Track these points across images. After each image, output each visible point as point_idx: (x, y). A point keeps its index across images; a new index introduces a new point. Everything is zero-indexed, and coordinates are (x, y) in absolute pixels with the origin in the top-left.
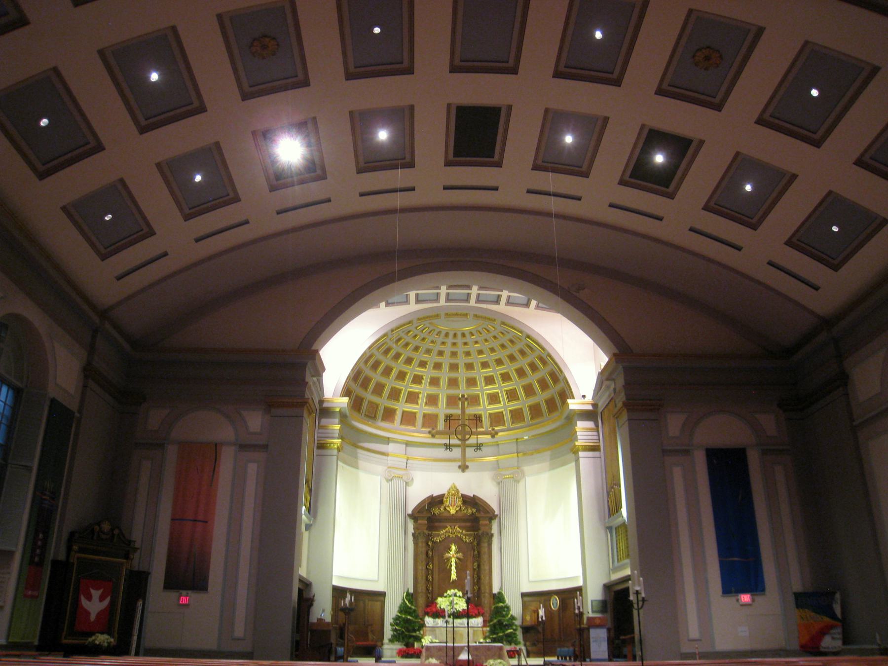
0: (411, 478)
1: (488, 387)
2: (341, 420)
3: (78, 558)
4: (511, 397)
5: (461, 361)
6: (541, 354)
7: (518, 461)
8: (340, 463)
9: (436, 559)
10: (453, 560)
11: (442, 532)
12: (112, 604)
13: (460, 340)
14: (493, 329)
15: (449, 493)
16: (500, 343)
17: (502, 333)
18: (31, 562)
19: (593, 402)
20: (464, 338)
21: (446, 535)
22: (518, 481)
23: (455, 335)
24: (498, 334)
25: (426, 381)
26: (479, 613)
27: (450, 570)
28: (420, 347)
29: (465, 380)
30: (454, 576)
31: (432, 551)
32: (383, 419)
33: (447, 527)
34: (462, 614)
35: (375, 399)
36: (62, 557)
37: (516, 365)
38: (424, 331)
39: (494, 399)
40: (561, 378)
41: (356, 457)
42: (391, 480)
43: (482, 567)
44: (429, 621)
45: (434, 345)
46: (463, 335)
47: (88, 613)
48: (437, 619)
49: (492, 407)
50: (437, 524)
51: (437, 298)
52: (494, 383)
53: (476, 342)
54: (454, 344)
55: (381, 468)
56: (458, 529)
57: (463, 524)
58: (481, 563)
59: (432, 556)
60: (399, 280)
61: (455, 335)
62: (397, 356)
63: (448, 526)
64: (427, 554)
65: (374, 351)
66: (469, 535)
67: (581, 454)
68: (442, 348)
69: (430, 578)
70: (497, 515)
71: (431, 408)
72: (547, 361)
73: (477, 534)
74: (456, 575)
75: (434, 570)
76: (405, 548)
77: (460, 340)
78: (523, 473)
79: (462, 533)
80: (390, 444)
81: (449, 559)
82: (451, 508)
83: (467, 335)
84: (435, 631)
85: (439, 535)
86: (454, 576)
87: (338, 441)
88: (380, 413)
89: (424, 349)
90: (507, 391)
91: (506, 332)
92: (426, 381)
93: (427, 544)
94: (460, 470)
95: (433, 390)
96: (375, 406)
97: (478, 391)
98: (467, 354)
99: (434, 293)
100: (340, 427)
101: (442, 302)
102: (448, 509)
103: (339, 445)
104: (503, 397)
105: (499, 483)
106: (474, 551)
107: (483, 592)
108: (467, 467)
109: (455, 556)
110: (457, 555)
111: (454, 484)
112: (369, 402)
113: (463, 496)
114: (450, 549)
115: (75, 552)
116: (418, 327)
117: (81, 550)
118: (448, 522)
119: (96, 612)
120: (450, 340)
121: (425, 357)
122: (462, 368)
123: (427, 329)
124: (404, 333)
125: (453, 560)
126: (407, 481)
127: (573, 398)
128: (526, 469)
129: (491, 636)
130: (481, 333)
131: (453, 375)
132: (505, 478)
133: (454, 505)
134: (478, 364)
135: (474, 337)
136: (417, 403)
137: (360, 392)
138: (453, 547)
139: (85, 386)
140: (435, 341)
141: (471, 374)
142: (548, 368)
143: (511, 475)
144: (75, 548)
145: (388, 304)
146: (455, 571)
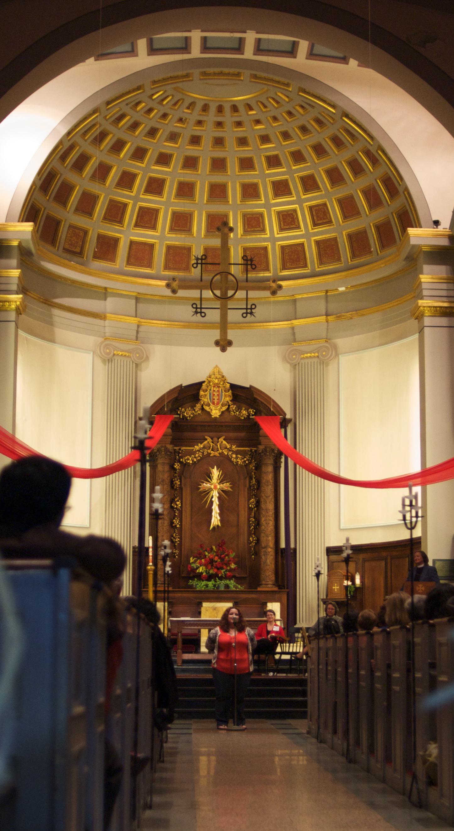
2: (21, 259)
4: (318, 217)
6: (368, 146)
8: (20, 332)
9: (187, 493)
11: (197, 448)
13: (228, 118)
14: (287, 99)
16: (300, 123)
17: (302, 107)
19: (451, 233)
20: (236, 114)
21: (203, 453)
23: (220, 109)
25: (170, 189)
31: (181, 479)
32: (96, 256)
33: (206, 439)
35: (81, 221)
38: (165, 103)
40: (401, 189)
41: (51, 323)
43: (263, 506)
45: (184, 126)
46: (235, 108)
50: (188, 434)
51: (185, 47)
52: (289, 193)
53: (258, 122)
55: (91, 340)
56: (224, 442)
57: (232, 435)
58: (262, 500)
59: (181, 488)
60: (105, 25)
61: (220, 109)
62: (118, 146)
63: (206, 437)
64: (172, 482)
65: (56, 164)
66: (243, 454)
67: (427, 321)
68: (197, 131)
69: (176, 522)
70: (290, 420)
71: (179, 236)
72: (379, 158)
73: (256, 451)
74: (219, 518)
75: (183, 510)
77: (228, 118)
79: (230, 450)
80: (109, 299)
82: (212, 406)
83: (241, 108)
85: (192, 453)
87: (16, 299)
88: (91, 246)
89: (167, 133)
90: (311, 208)
91: (310, 105)
92: (170, 189)
93: (172, 468)
94: (218, 349)
95: (182, 205)
96: (82, 234)
98: (243, 142)
99: (182, 37)
100: (21, 273)
101: (196, 52)
102: (207, 408)
103: (18, 303)
105: (294, 366)
106: (251, 478)
107: (263, 545)
108: (230, 343)
109: (218, 487)
110: (221, 485)
111: (217, 366)
112: (71, 226)
113: (233, 387)
114: (208, 477)
116: (153, 95)
121: (168, 147)
122: (233, 166)
123: (170, 98)
124: (130, 105)
127: (418, 225)
129: (180, 634)
130: (265, 107)
131: (218, 178)
132: (303, 358)
133: (218, 403)
134: (261, 158)
135: (254, 112)
136: (154, 227)
137: (56, 210)
138: (215, 473)
140: (186, 119)
141: (250, 176)
142: (381, 171)
143: (314, 353)
146: (218, 511)
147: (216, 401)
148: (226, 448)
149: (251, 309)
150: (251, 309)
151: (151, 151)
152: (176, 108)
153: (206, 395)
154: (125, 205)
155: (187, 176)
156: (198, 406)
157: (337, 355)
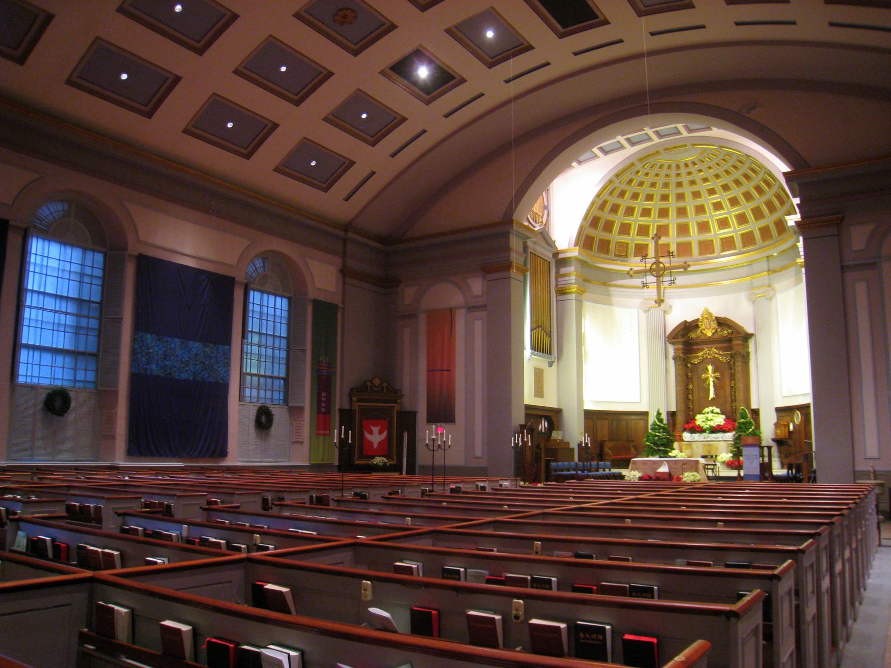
0: (669, 306)
1: (716, 213)
3: (359, 406)
5: (687, 190)
7: (769, 279)
10: (711, 380)
11: (700, 354)
12: (389, 436)
13: (683, 171)
15: (702, 317)
18: (319, 412)
20: (688, 168)
22: (770, 299)
24: (719, 161)
25: (654, 213)
26: (734, 427)
27: (709, 390)
28: (645, 182)
29: (693, 209)
30: (712, 395)
34: (716, 429)
35: (624, 239)
36: (346, 406)
37: (743, 189)
38: (646, 167)
39: (724, 223)
41: (609, 295)
42: (648, 311)
44: (686, 436)
46: (686, 165)
47: (371, 443)
48: (694, 435)
49: (722, 231)
50: (695, 347)
53: (700, 171)
54: (678, 175)
55: (637, 301)
56: (715, 350)
57: (719, 345)
59: (692, 377)
61: (678, 167)
64: (687, 375)
69: (690, 396)
76: (667, 371)
77: (683, 171)
78: (773, 289)
81: (707, 379)
82: (707, 330)
84: (691, 445)
85: (697, 357)
86: (712, 395)
92: (654, 213)
97: (707, 217)
98: (693, 183)
102: (704, 332)
104: (733, 221)
105: (754, 302)
109: (713, 375)
113: (717, 319)
115: (355, 402)
117: (359, 400)
118: (705, 344)
119: (377, 443)
120: (673, 172)
122: (688, 197)
124: (632, 174)
125: (711, 380)
126: (665, 310)
128: (776, 286)
138: (710, 368)
139: (344, 284)
144: (354, 399)
145: (580, 163)
147: (708, 327)
148: (716, 353)
149: (673, 280)
150: (673, 280)
151: (641, 194)
152: (653, 169)
153: (702, 325)
154: (630, 225)
155: (663, 204)
156: (698, 332)
157: (775, 294)
